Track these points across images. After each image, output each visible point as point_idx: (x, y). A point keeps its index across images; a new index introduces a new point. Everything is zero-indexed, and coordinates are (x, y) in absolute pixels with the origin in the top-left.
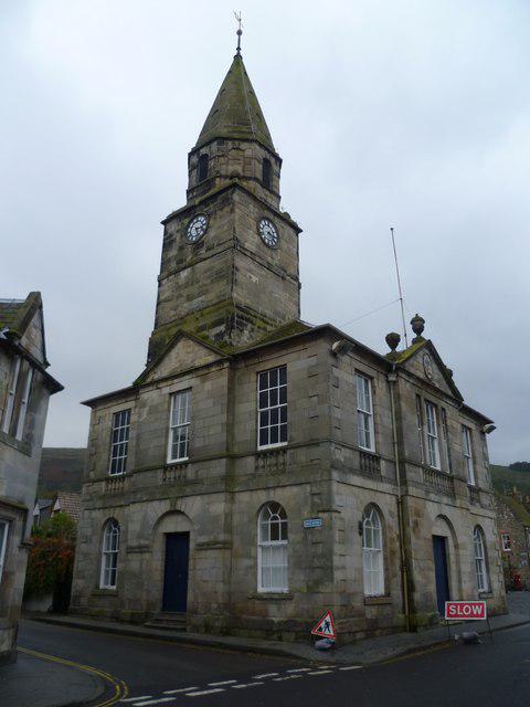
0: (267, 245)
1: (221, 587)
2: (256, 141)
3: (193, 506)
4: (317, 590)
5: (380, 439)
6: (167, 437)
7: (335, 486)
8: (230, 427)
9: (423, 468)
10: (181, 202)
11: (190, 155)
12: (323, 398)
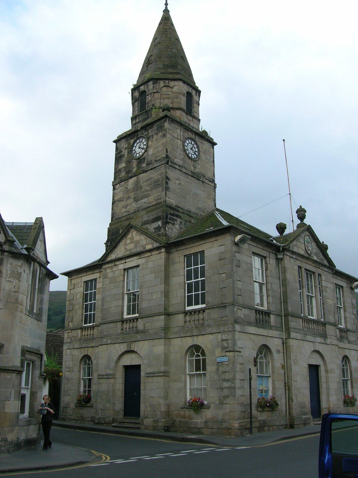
0: (190, 158)
1: (162, 401)
2: (181, 80)
3: (143, 347)
4: (225, 402)
5: (271, 299)
6: (123, 299)
7: (237, 335)
8: (167, 294)
9: (302, 318)
10: (127, 127)
11: (133, 90)
12: (230, 276)
